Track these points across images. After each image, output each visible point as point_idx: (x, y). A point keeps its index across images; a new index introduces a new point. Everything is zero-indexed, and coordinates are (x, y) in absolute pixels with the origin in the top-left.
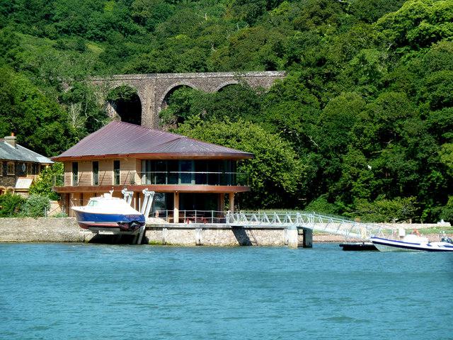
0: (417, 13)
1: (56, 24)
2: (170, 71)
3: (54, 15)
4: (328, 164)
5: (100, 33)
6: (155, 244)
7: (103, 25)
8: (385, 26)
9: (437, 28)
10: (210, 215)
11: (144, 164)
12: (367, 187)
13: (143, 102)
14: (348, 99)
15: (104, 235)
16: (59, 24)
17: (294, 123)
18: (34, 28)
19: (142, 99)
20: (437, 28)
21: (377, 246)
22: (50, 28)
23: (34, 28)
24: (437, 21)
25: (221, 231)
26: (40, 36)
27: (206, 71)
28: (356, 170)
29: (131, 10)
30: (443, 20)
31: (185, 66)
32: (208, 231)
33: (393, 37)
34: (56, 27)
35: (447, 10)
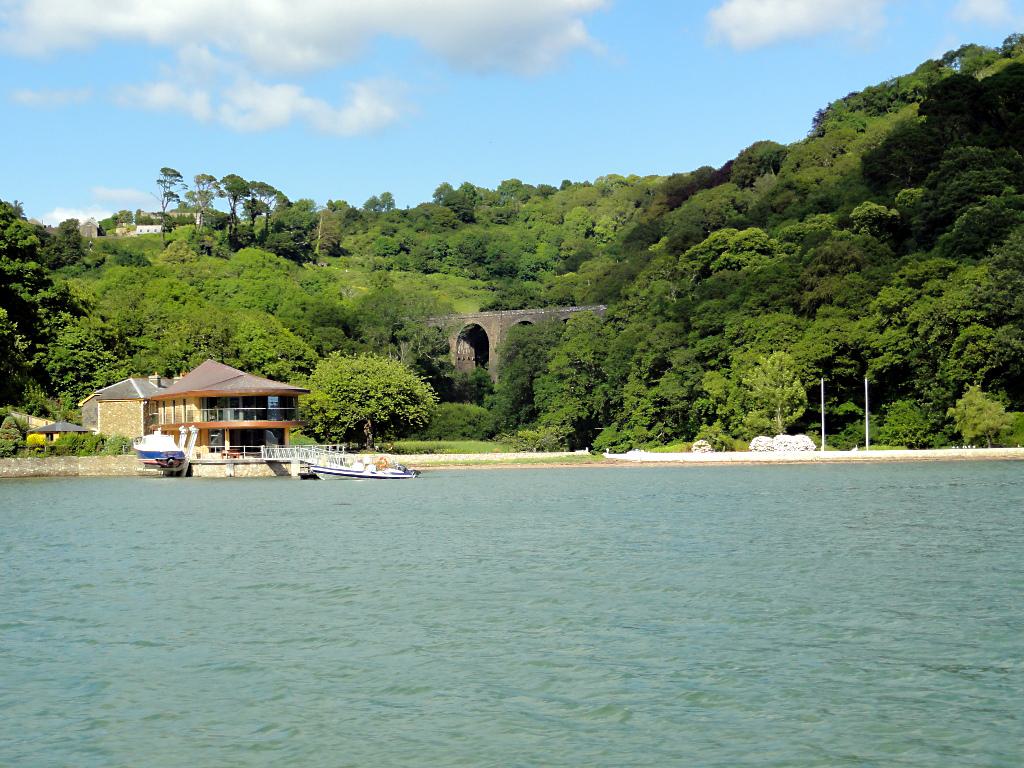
0: (719, 244)
1: (487, 266)
2: (521, 308)
3: (485, 258)
4: (614, 395)
5: (532, 273)
6: (43, 475)
7: (533, 266)
8: (692, 257)
9: (736, 258)
10: (242, 450)
11: (205, 401)
12: (646, 416)
13: (490, 339)
14: (638, 331)
15: (926, 458)
16: (491, 266)
17: (585, 354)
18: (466, 270)
19: (489, 335)
20: (736, 258)
21: (318, 474)
22: (481, 270)
23: (466, 270)
24: (737, 251)
25: (255, 466)
26: (473, 278)
27: (573, 305)
28: (636, 399)
29: (560, 250)
30: (742, 250)
31: (539, 303)
32: (240, 466)
33: (698, 269)
34: (488, 269)
35: (746, 239)
